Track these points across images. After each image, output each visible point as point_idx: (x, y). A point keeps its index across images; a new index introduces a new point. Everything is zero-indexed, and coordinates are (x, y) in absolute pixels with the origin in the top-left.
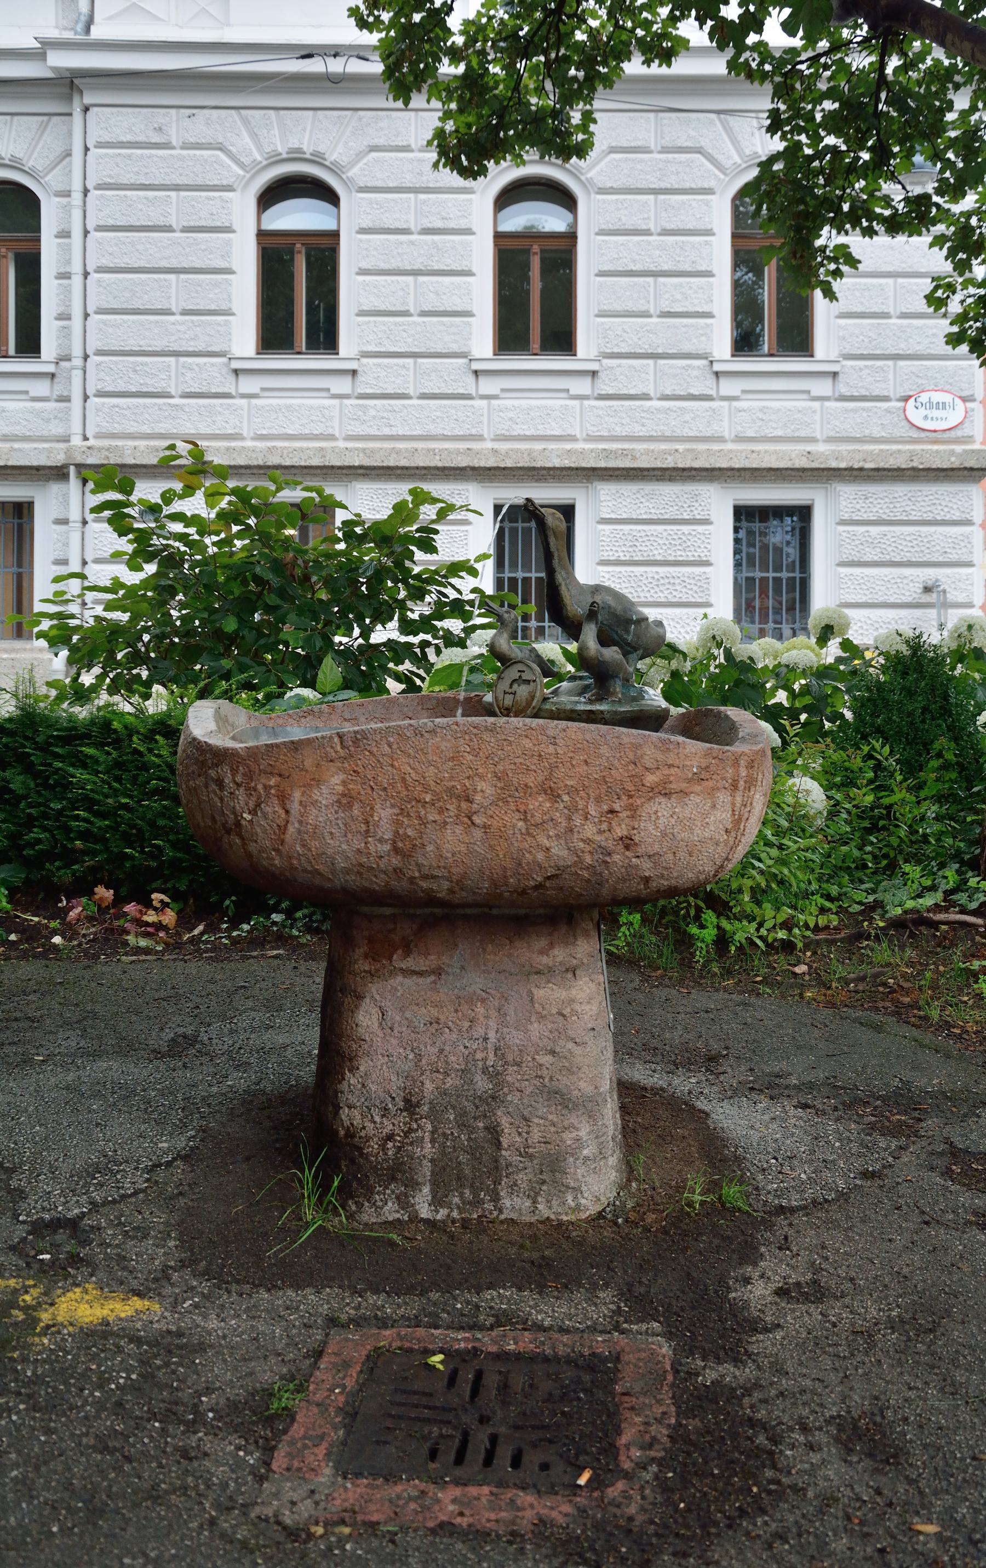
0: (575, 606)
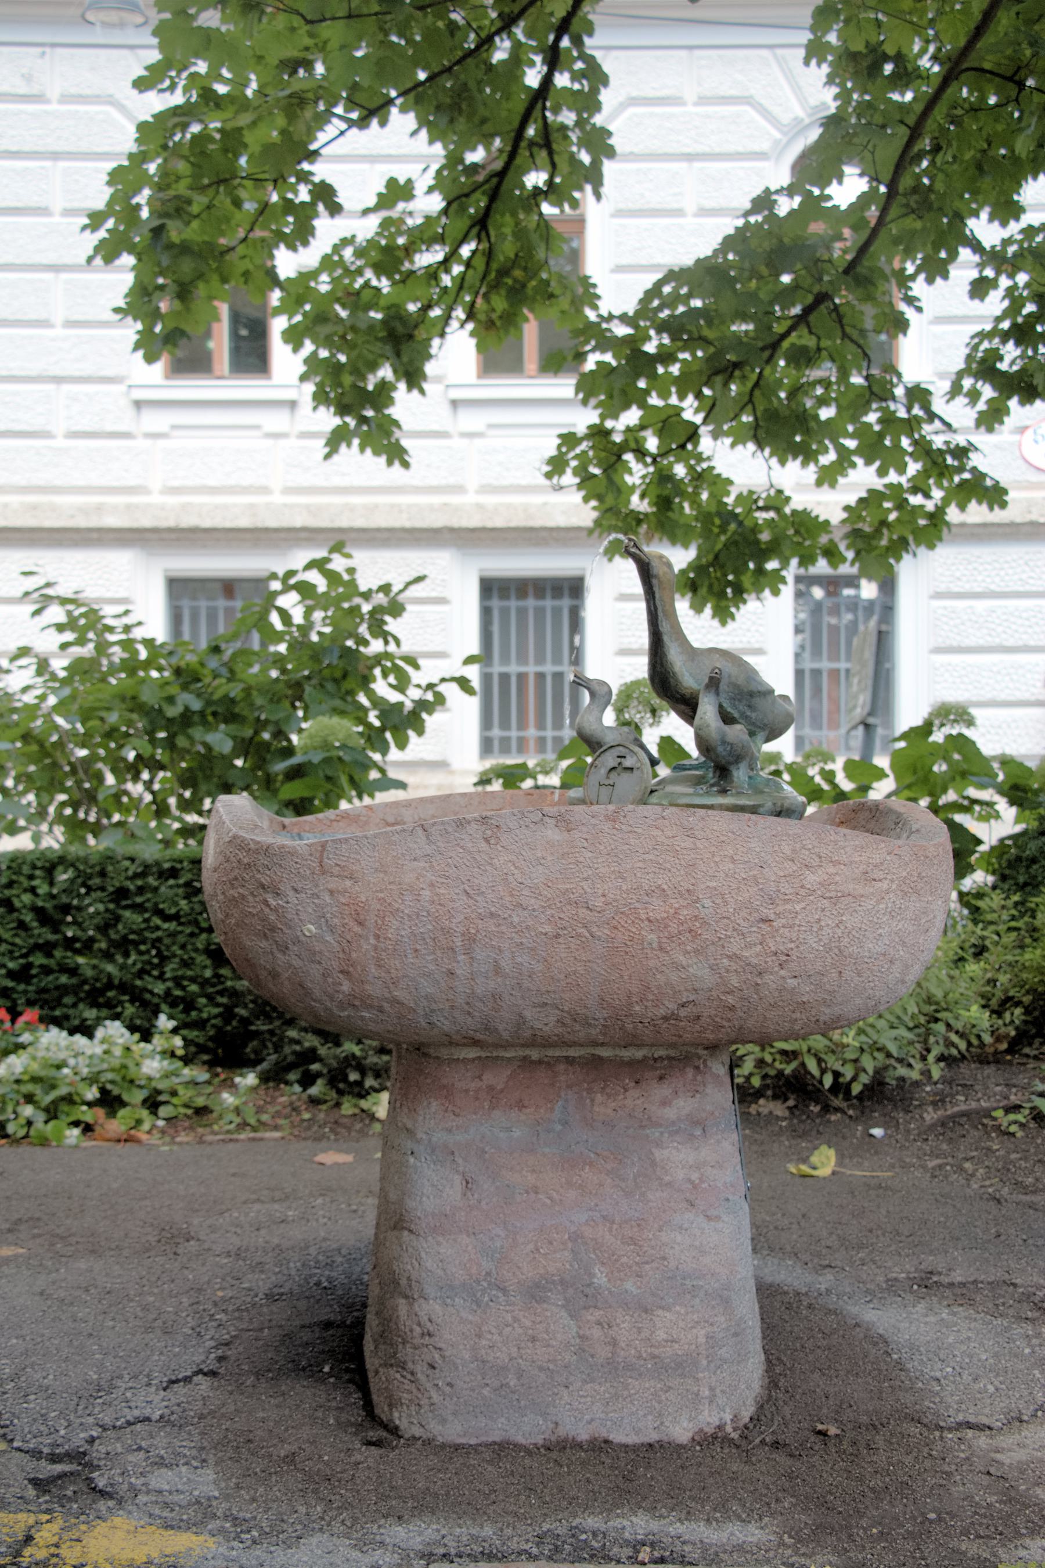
0: (688, 678)
